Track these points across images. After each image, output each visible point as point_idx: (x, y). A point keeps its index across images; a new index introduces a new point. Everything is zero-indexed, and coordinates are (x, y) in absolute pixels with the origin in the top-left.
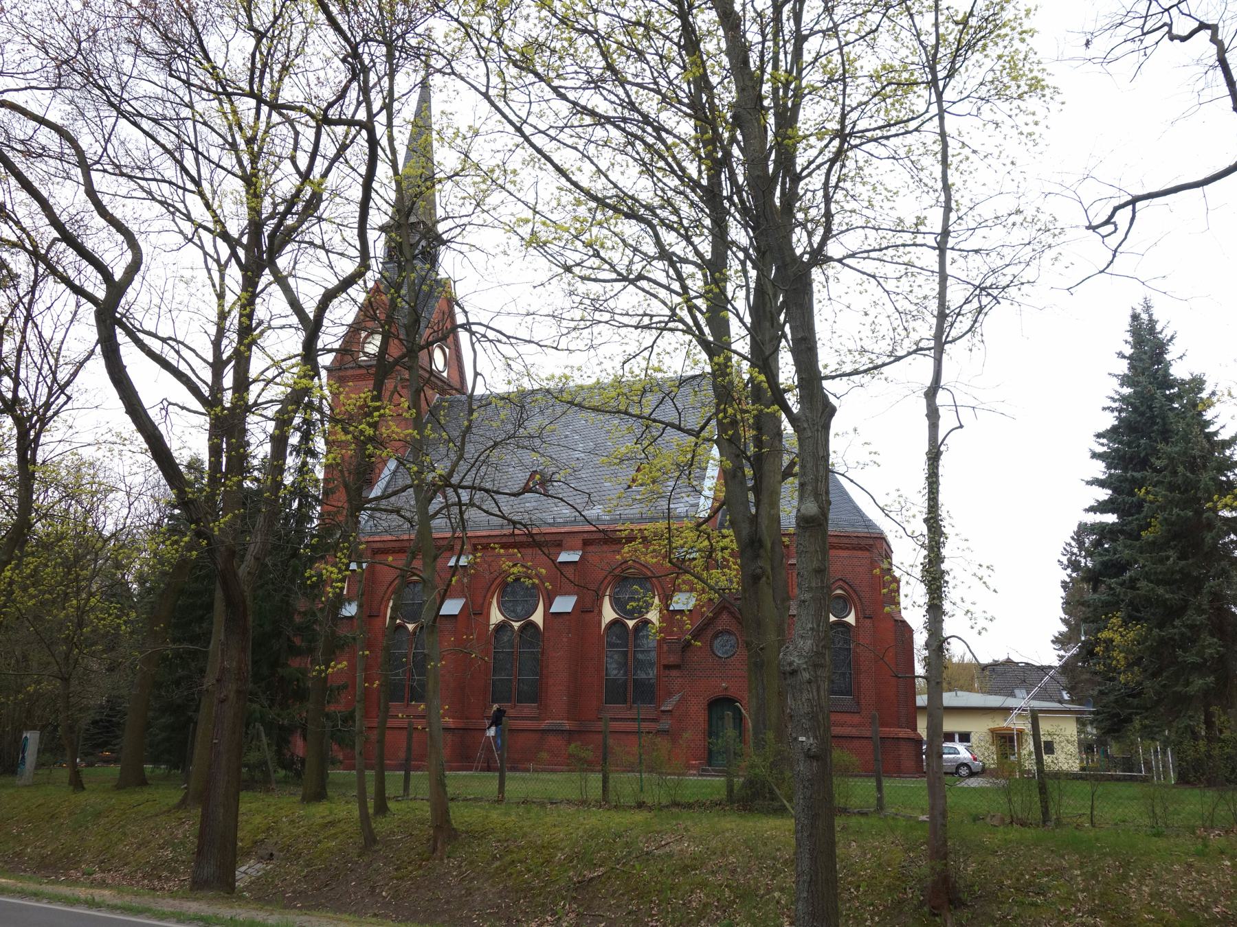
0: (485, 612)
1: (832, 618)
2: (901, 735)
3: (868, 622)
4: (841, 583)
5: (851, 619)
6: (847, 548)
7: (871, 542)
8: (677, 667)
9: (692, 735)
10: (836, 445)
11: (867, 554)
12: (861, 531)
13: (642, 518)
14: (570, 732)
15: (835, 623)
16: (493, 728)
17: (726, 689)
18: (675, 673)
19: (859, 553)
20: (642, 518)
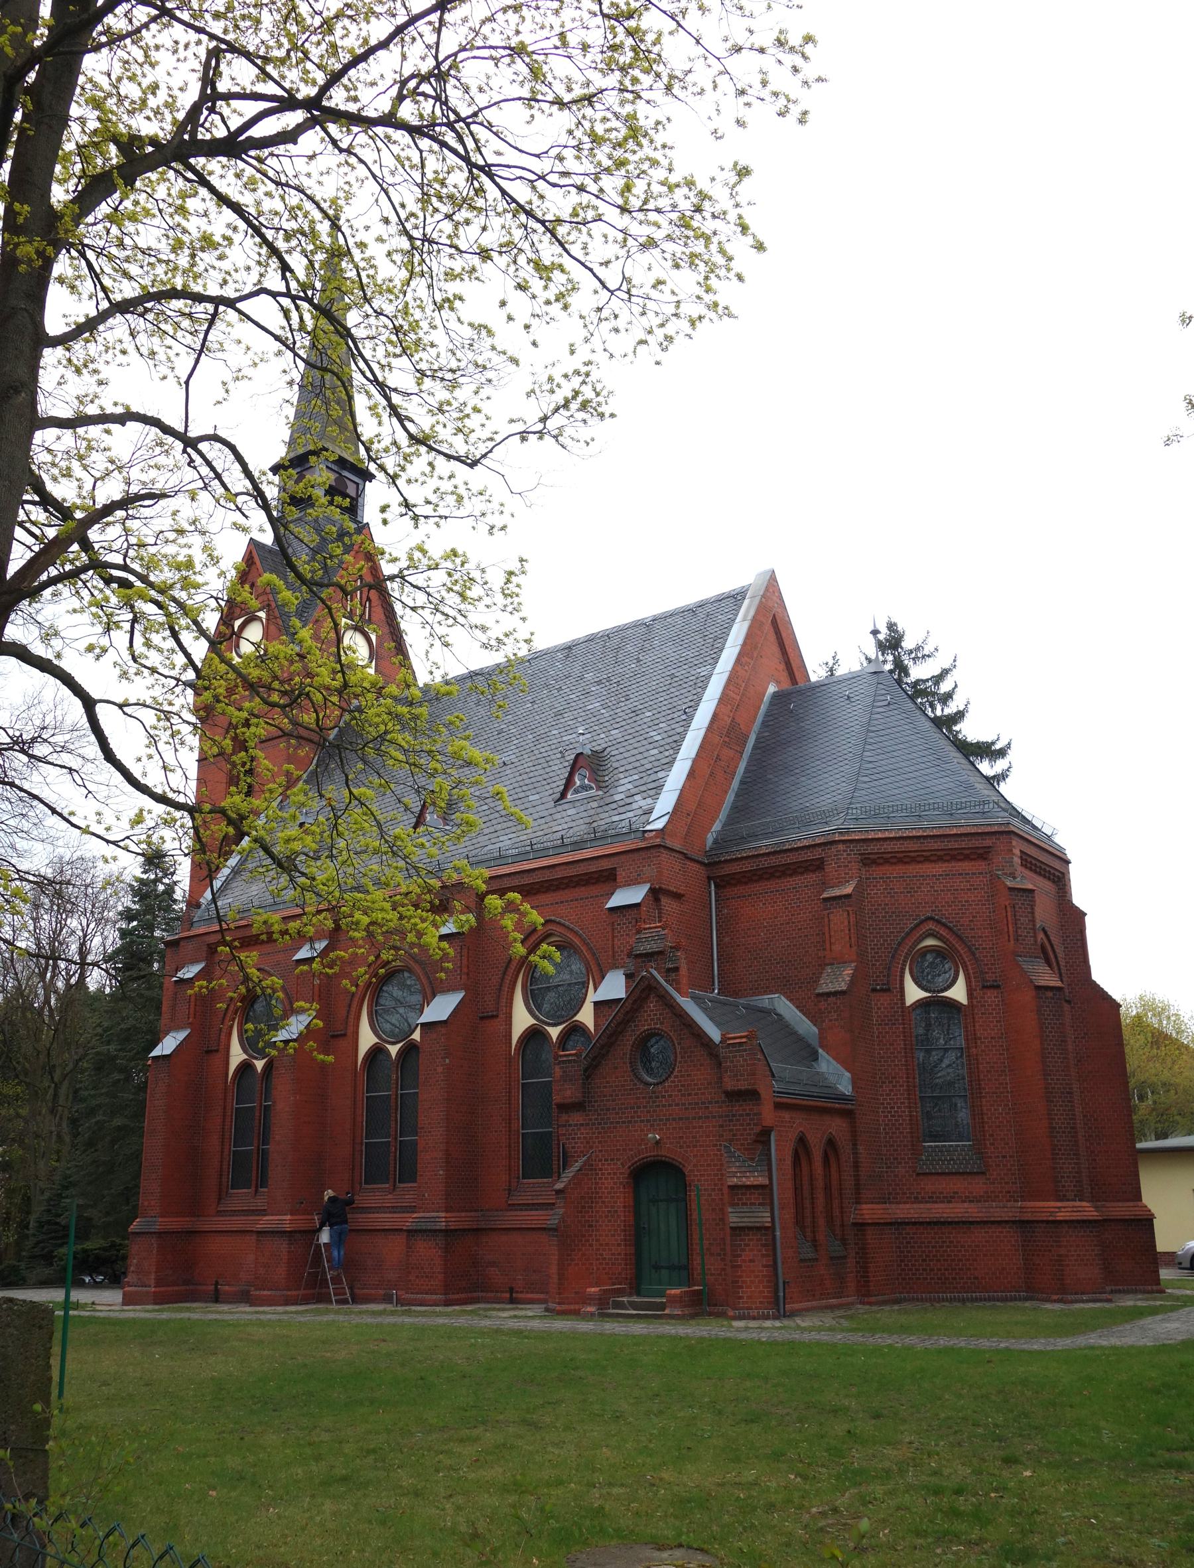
0: (350, 1031)
1: (914, 993)
2: (1061, 1216)
3: (991, 997)
4: (931, 925)
5: (958, 992)
6: (940, 859)
7: (988, 842)
8: (578, 1106)
9: (609, 1237)
10: (13, 659)
11: (981, 866)
12: (1002, 818)
13: (563, 845)
14: (447, 1232)
15: (921, 1004)
16: (326, 1229)
17: (658, 1142)
18: (576, 1118)
19: (966, 866)
20: (563, 845)
